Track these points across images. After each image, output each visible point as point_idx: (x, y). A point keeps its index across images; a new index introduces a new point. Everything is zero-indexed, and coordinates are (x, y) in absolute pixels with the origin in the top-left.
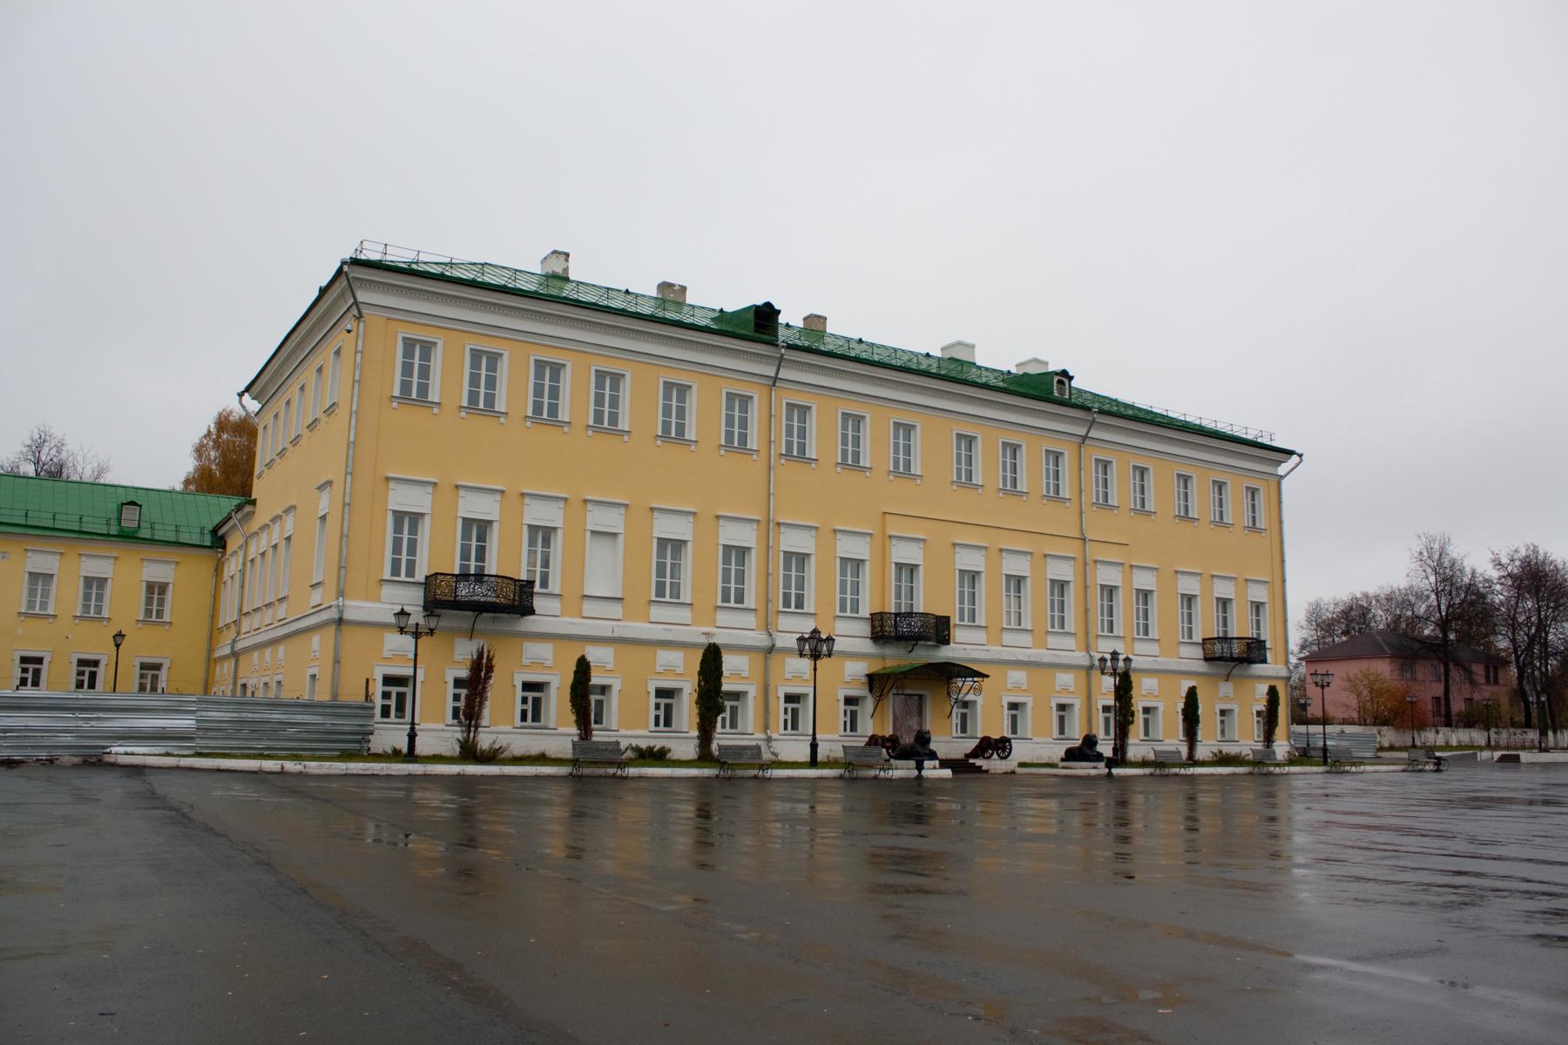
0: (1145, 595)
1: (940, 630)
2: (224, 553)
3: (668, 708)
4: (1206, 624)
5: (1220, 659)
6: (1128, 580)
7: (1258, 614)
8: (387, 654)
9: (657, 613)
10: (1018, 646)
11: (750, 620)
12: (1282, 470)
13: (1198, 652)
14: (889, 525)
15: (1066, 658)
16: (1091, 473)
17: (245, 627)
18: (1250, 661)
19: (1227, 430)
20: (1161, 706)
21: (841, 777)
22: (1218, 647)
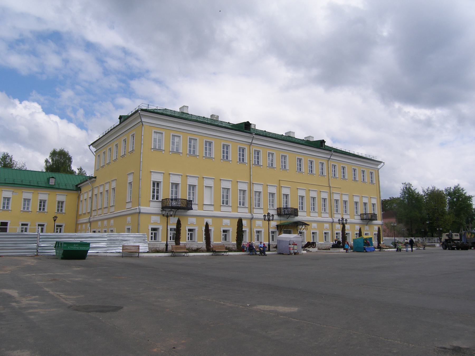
0: (345, 202)
1: (295, 212)
2: (81, 193)
3: (191, 235)
4: (361, 210)
5: (366, 219)
6: (341, 198)
7: (345, 204)
8: (152, 222)
9: (223, 209)
10: (314, 216)
11: (247, 210)
12: (379, 167)
13: (359, 217)
14: (279, 184)
15: (326, 219)
16: (331, 169)
17: (94, 213)
18: (371, 220)
19: (361, 155)
20: (197, 228)
21: (171, 256)
22: (365, 216)
